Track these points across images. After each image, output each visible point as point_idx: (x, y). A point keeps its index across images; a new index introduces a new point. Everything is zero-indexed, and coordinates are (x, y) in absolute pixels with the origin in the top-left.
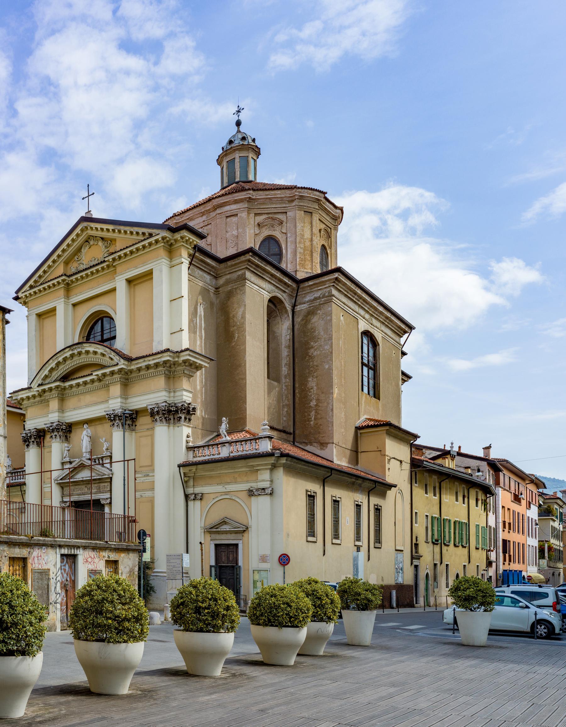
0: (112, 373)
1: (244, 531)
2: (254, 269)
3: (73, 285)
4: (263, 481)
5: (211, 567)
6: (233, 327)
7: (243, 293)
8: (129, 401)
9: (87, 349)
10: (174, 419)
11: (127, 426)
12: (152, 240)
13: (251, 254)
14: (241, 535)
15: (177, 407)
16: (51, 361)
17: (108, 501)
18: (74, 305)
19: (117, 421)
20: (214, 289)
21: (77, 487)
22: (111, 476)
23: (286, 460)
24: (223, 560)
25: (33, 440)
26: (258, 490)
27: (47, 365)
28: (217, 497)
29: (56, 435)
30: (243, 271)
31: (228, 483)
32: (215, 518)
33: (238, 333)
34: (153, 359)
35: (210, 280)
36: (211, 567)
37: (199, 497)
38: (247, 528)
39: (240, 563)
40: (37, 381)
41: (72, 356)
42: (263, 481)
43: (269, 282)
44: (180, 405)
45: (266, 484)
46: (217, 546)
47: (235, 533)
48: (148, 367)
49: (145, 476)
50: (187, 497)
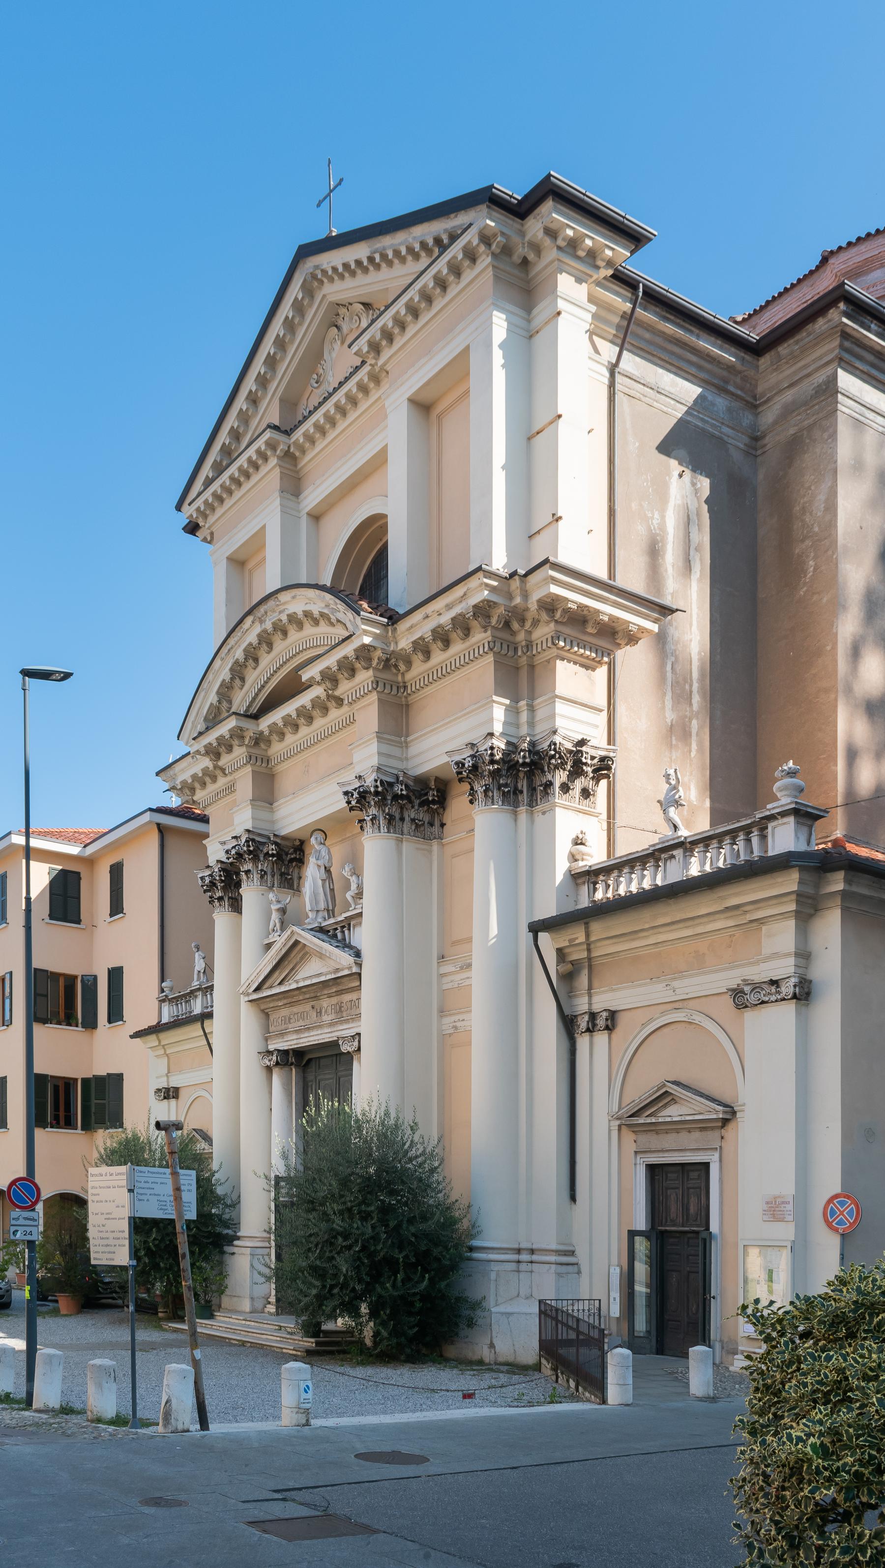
0: (348, 668)
1: (725, 1122)
2: (873, 365)
3: (307, 458)
4: (775, 956)
5: (632, 1234)
6: (803, 541)
7: (830, 436)
8: (413, 750)
10: (532, 789)
11: (407, 826)
12: (456, 251)
13: (842, 306)
14: (717, 1134)
15: (537, 753)
16: (218, 663)
17: (356, 1043)
18: (316, 517)
19: (373, 811)
20: (746, 440)
22: (355, 969)
23: (847, 881)
24: (673, 1215)
25: (219, 894)
26: (757, 987)
27: (210, 676)
28: (651, 1020)
29: (247, 872)
30: (829, 370)
31: (679, 974)
32: (640, 1089)
33: (815, 558)
34: (449, 607)
35: (729, 410)
36: (632, 1234)
37: (601, 1022)
38: (734, 1113)
39: (714, 1227)
40: (194, 726)
42: (775, 956)
44: (545, 746)
45: (784, 968)
46: (652, 1169)
47: (702, 1129)
48: (443, 638)
49: (462, 968)
50: (568, 1023)
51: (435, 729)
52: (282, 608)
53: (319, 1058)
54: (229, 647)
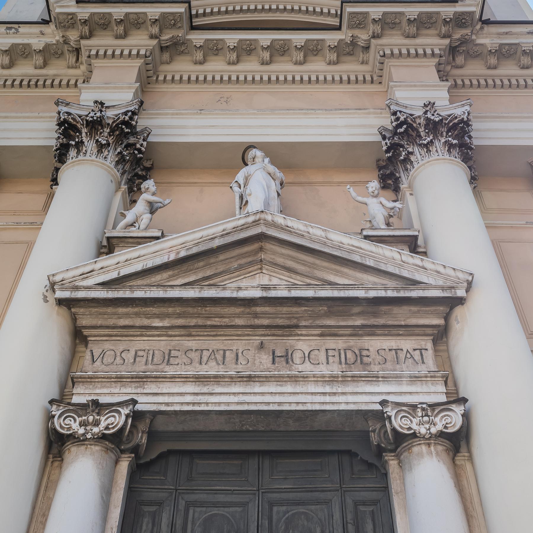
21: (192, 343)
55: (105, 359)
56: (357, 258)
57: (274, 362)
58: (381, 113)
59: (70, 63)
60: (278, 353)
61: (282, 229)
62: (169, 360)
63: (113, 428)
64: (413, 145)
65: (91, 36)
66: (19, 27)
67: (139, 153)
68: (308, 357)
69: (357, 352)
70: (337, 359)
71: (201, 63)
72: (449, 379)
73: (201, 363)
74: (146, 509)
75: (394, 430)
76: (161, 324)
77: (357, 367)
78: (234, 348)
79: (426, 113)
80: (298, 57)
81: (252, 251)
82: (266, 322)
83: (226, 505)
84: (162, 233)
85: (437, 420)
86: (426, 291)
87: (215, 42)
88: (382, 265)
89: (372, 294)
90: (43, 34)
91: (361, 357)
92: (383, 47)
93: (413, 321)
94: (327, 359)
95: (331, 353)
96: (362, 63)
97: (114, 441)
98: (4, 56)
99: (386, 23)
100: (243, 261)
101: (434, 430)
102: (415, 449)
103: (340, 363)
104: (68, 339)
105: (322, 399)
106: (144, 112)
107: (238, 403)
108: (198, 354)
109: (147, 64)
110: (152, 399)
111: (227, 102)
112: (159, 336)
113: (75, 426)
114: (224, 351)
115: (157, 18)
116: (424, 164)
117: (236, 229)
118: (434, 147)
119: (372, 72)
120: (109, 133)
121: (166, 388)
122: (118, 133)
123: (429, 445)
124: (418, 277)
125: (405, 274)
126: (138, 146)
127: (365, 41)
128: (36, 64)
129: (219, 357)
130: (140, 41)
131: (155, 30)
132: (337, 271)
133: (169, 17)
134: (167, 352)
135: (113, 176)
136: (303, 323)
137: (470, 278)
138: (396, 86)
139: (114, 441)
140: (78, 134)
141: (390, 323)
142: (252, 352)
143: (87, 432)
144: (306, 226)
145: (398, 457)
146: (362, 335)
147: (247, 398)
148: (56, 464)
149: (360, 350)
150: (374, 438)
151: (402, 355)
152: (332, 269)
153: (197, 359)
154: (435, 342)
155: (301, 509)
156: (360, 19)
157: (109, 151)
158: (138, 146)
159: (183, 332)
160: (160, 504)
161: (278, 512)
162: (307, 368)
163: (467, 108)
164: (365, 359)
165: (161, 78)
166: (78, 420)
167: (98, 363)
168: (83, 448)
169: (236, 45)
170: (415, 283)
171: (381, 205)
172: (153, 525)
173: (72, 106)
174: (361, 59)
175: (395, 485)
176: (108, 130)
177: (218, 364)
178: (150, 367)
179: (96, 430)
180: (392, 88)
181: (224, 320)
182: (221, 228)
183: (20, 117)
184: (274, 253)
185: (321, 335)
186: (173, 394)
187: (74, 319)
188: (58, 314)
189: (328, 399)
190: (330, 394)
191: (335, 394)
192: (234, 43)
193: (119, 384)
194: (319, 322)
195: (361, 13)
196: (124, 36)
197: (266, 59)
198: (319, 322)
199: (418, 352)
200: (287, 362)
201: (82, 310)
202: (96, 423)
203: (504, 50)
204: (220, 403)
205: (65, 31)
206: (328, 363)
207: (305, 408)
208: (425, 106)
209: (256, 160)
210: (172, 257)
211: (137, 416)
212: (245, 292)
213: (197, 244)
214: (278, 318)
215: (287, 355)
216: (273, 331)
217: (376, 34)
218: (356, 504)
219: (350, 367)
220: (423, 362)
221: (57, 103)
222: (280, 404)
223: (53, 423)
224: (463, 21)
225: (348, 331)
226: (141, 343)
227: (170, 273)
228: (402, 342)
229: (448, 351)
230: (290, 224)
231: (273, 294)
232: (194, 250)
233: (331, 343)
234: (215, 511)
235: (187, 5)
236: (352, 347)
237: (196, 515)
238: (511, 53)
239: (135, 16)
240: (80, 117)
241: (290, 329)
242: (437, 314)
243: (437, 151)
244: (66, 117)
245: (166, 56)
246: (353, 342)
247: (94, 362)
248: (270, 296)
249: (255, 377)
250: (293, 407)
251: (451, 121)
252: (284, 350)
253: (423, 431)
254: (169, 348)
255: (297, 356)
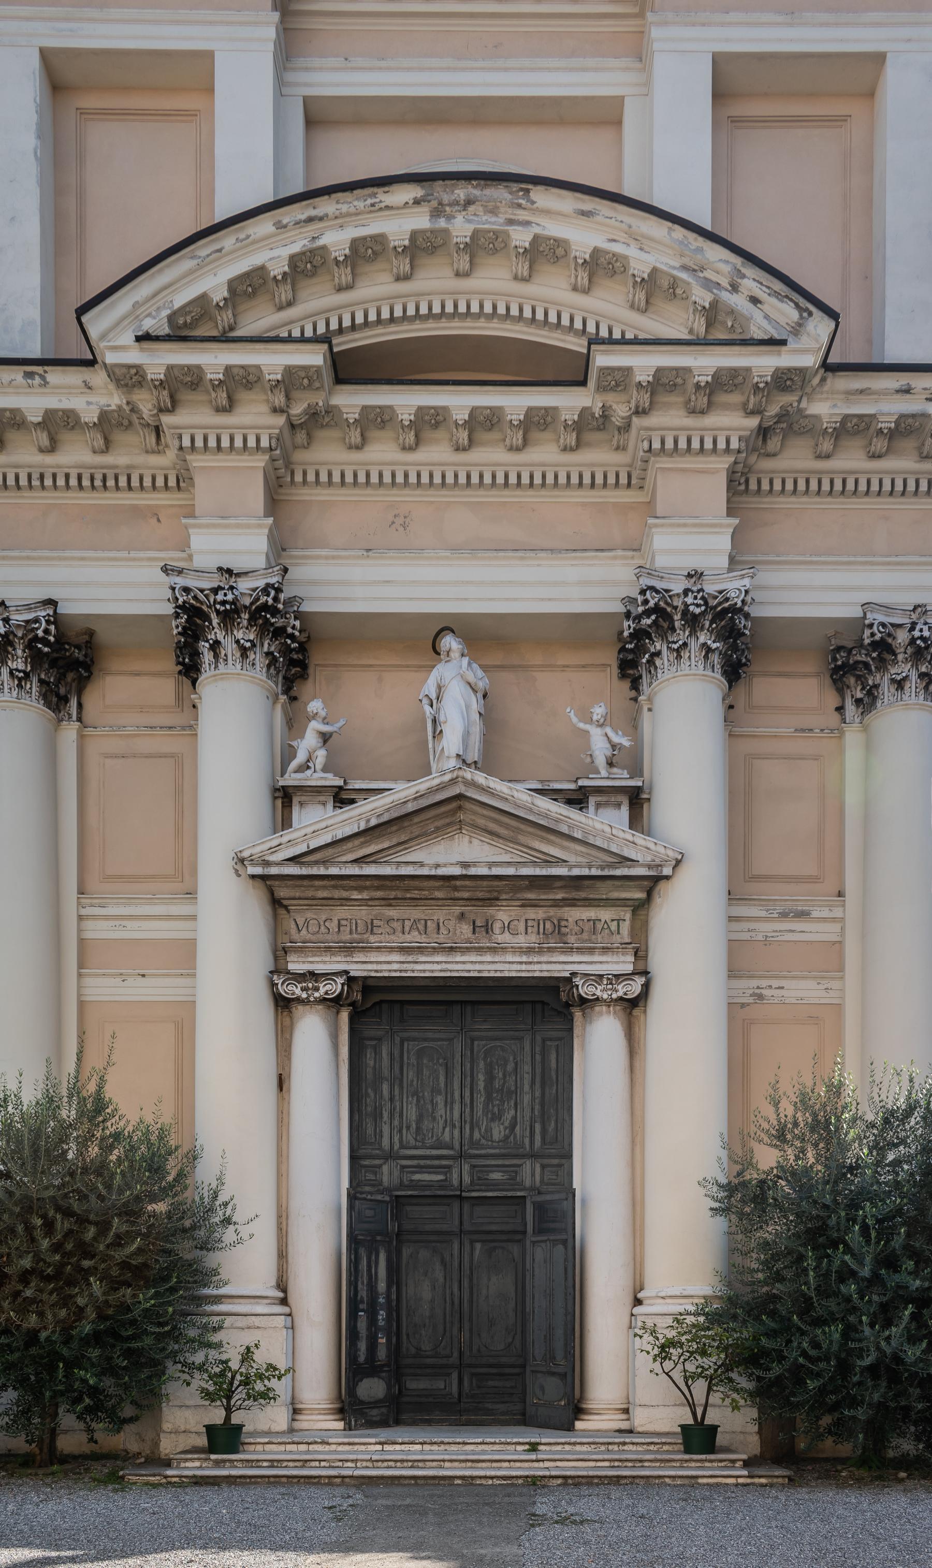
9: (553, 229)
16: (263, 226)
21: (392, 913)
27: (227, 240)
39: (576, 1184)
41: (421, 248)
43: (866, 563)
51: (811, 563)
52: (522, 215)
53: (402, 1003)
54: (312, 213)
55: (310, 929)
56: (564, 829)
57: (474, 932)
58: (633, 558)
59: (148, 445)
60: (478, 923)
61: (483, 789)
62: (372, 930)
63: (332, 994)
64: (663, 640)
65: (174, 406)
66: (45, 372)
67: (293, 642)
68: (507, 928)
69: (556, 922)
70: (536, 929)
71: (358, 448)
72: (641, 954)
73: (403, 933)
74: (368, 1043)
75: (580, 995)
76: (360, 897)
77: (556, 936)
78: (435, 918)
79: (686, 592)
80: (514, 439)
81: (450, 811)
82: (466, 895)
83: (434, 1040)
84: (345, 781)
85: (620, 987)
86: (631, 869)
87: (378, 410)
88: (591, 837)
89: (576, 872)
90: (89, 388)
91: (559, 928)
92: (650, 433)
93: (615, 895)
94: (526, 929)
95: (530, 923)
96: (617, 448)
97: (335, 1003)
98: (39, 432)
99: (662, 385)
100: (439, 823)
101: (614, 996)
102: (597, 1009)
103: (539, 933)
104: (268, 909)
105: (518, 967)
106: (284, 553)
107: (441, 971)
108: (400, 923)
109: (274, 460)
110: (362, 966)
111: (404, 526)
112: (359, 906)
113: (298, 991)
114: (426, 921)
115: (279, 377)
116: (668, 680)
117: (431, 791)
118: (687, 651)
119: (630, 466)
120: (249, 620)
121: (373, 957)
122: (261, 621)
123: (609, 1006)
124: (626, 853)
125: (614, 849)
126: (290, 630)
127: (623, 418)
128: (93, 447)
129: (421, 927)
130: (256, 417)
131: (279, 399)
132: (543, 838)
133: (299, 373)
134: (369, 922)
135: (267, 690)
136: (504, 896)
137: (680, 857)
138: (656, 526)
139: (335, 1003)
140: (207, 623)
141: (591, 896)
142: (453, 922)
143: (309, 996)
144: (510, 788)
145: (583, 1010)
146: (562, 906)
147: (450, 967)
148: (285, 1013)
149: (559, 921)
150: (564, 997)
151: (599, 926)
152: (537, 836)
153: (400, 929)
154: (634, 912)
155: (498, 1043)
156: (617, 378)
157: (255, 653)
158: (290, 630)
159: (383, 902)
160: (379, 1039)
161: (478, 1045)
162: (505, 938)
163: (747, 582)
164: (563, 930)
165: (299, 478)
166: (299, 986)
167: (304, 932)
168: (308, 1007)
169: (412, 417)
170: (625, 860)
171: (606, 738)
172: (376, 1055)
173: (187, 574)
174: (615, 443)
175: (577, 1031)
176: (247, 616)
177: (420, 933)
178: (355, 936)
179: (317, 995)
180: (650, 528)
181: (424, 893)
182: (413, 790)
183: (103, 559)
184: (475, 813)
185: (522, 906)
186: (381, 963)
187: (272, 893)
188: (254, 888)
189: (524, 967)
190: (526, 963)
191: (531, 963)
192: (410, 414)
193: (329, 954)
194: (519, 896)
195: (619, 369)
196: (229, 407)
197: (463, 444)
198: (519, 896)
199: (615, 923)
200: (487, 932)
201: (277, 883)
202: (317, 989)
203: (849, 424)
204: (424, 971)
205: (129, 393)
206: (526, 933)
207: (502, 975)
208: (689, 576)
209: (452, 654)
210: (363, 826)
211: (351, 980)
212: (444, 869)
213: (388, 810)
214: (476, 893)
215: (487, 925)
216: (473, 903)
217: (640, 409)
218: (544, 1040)
219: (548, 938)
220: (619, 933)
221: (166, 570)
222: (479, 971)
223: (277, 989)
224: (788, 383)
225: (550, 903)
226: (342, 912)
227: (362, 840)
228: (602, 912)
229: (647, 915)
230: (492, 785)
231: (473, 871)
232: (385, 818)
233: (531, 913)
234: (426, 1044)
235: (326, 346)
236: (551, 917)
237: (410, 1047)
238: (860, 428)
239: (241, 372)
240: (202, 591)
241: (491, 901)
242: (641, 889)
243: (689, 657)
244: (185, 598)
245: (301, 437)
246: (552, 912)
247: (299, 931)
248: (469, 873)
249: (456, 947)
250: (492, 974)
251: (720, 603)
252: (484, 920)
253: (605, 996)
254: (370, 917)
255: (497, 926)
